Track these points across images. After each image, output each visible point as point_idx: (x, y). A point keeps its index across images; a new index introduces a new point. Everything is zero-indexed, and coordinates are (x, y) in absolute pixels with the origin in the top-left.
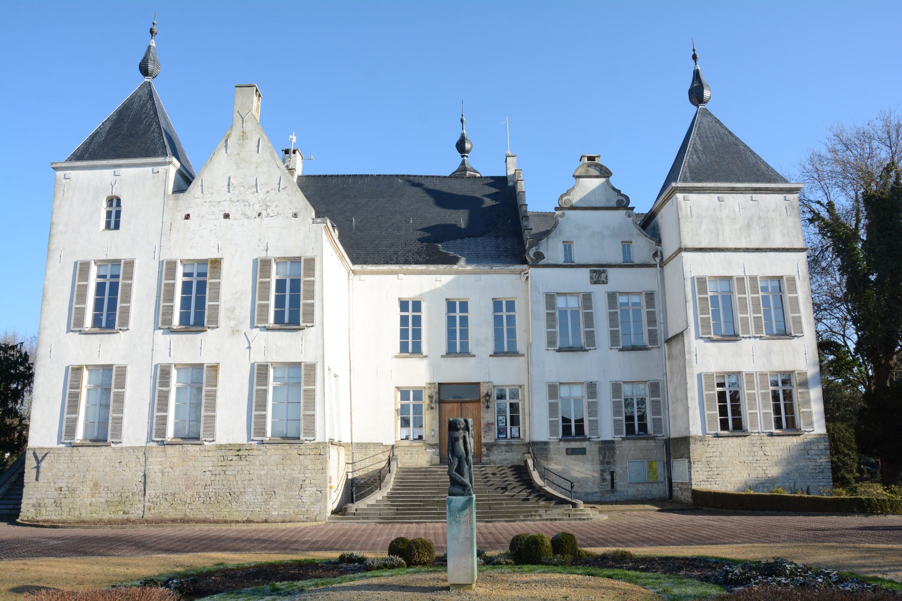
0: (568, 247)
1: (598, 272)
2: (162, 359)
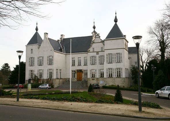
1: (98, 53)
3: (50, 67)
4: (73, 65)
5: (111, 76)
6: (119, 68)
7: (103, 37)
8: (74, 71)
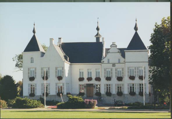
0: (109, 60)
1: (114, 65)
2: (29, 83)
5: (132, 93)
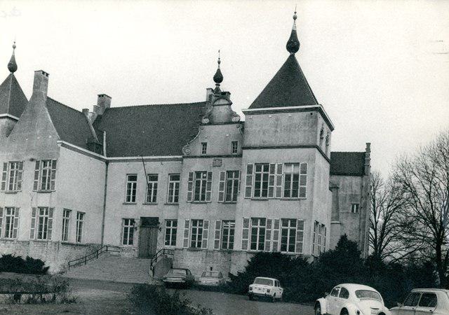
3: (44, 200)
4: (131, 196)
6: (293, 222)
7: (242, 101)
8: (133, 221)
